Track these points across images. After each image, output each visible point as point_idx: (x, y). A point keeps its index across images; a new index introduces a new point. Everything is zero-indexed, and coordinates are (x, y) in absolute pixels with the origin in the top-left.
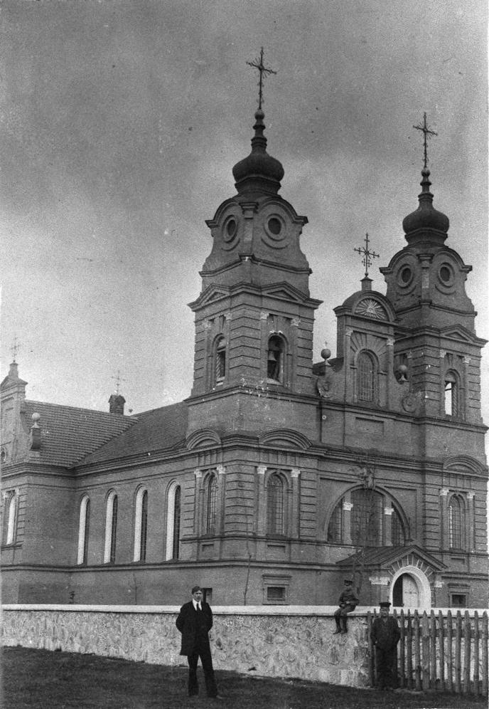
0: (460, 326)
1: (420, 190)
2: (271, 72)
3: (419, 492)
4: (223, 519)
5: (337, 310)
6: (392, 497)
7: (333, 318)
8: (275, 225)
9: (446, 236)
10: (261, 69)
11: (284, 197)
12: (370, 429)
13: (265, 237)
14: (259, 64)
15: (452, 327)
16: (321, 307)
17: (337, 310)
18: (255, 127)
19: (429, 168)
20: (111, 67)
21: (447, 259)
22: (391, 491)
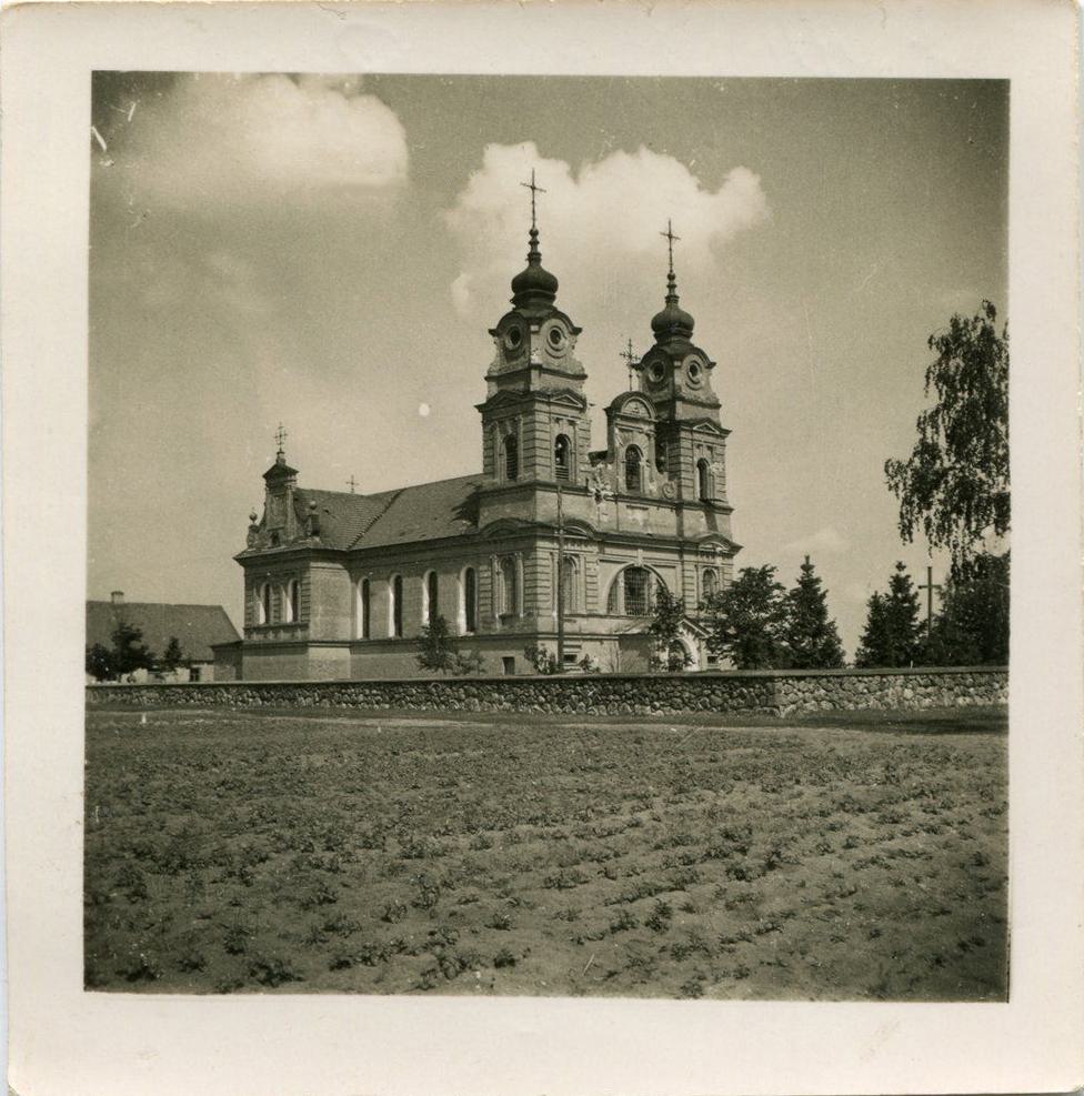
0: (709, 420)
1: (528, 249)
2: (524, 185)
3: (679, 568)
4: (386, 644)
5: (607, 410)
6: (658, 575)
7: (604, 417)
8: (555, 336)
9: (553, 298)
10: (533, 188)
11: (560, 309)
12: (639, 515)
13: (548, 348)
14: (536, 192)
15: (702, 421)
16: (731, 434)
17: (607, 410)
18: (530, 243)
19: (538, 227)
20: (926, 400)
21: (695, 358)
22: (657, 570)
